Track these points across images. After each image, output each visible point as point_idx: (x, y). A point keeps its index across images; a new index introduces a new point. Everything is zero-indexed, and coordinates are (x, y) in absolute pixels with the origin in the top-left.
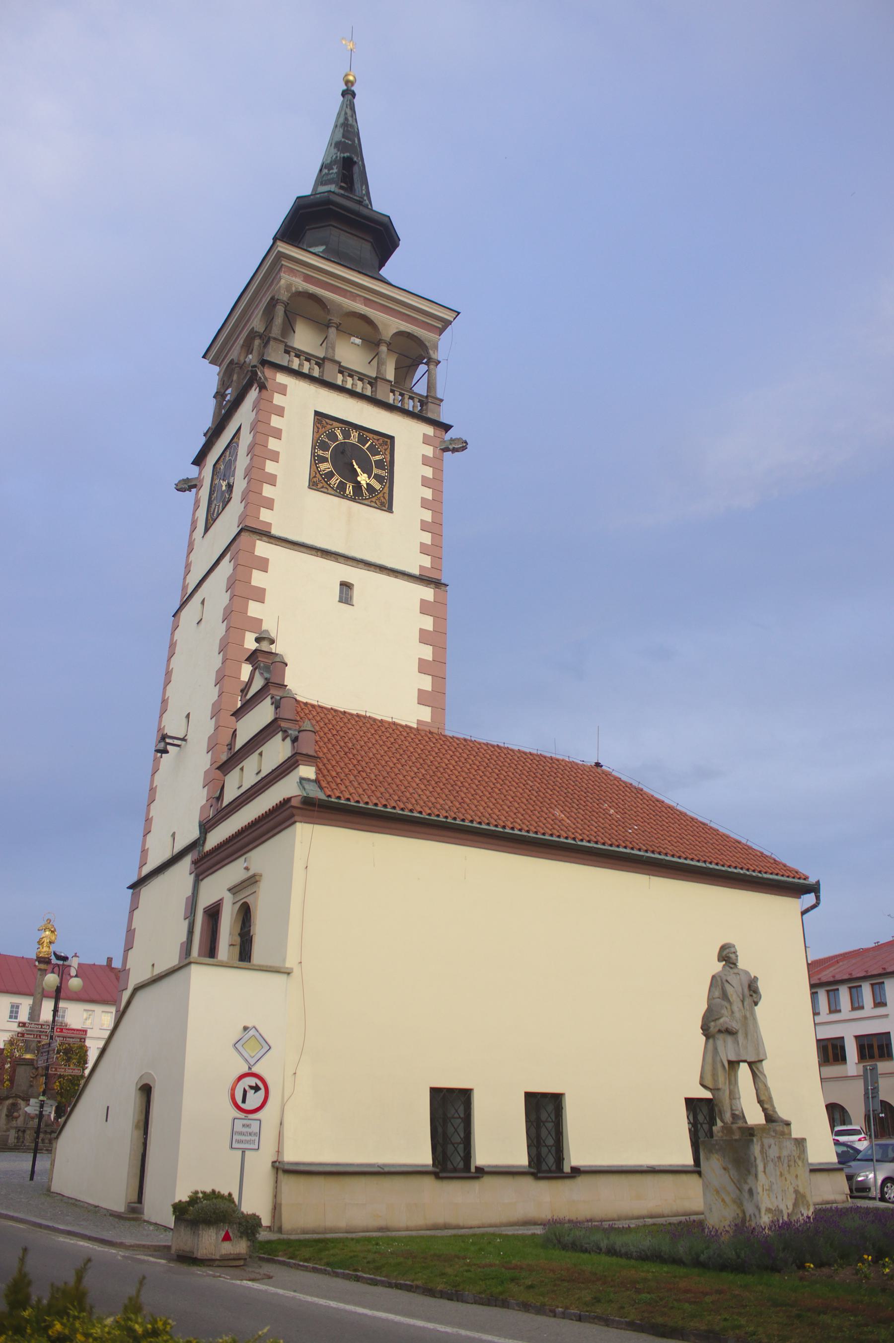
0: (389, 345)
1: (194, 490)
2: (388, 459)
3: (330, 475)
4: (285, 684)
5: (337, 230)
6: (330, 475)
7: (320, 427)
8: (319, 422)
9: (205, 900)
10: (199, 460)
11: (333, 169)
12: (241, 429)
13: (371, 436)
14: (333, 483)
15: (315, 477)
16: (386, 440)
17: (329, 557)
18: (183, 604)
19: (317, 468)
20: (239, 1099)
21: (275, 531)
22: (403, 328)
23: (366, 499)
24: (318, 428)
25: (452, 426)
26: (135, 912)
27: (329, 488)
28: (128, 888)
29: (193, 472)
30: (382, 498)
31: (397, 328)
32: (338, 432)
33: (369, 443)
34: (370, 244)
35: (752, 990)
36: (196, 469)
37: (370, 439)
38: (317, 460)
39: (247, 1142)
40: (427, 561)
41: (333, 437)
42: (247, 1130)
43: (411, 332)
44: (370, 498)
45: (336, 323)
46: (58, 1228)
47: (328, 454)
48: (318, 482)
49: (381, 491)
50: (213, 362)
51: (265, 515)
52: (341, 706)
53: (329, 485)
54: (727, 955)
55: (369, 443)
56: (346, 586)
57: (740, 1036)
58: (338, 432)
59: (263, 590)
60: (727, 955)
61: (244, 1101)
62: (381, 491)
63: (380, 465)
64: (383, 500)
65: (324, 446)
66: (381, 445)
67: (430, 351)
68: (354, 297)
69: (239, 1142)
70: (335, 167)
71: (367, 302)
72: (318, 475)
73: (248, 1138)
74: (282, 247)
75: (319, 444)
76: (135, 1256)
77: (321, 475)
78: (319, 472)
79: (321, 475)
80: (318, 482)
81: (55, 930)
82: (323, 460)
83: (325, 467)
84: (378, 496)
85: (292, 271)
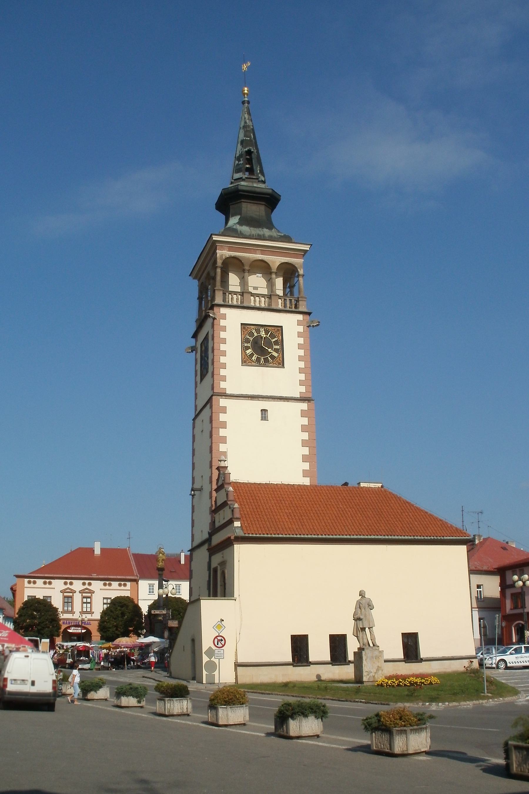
0: (276, 273)
1: (194, 352)
2: (255, 327)
3: (252, 355)
4: (93, 611)
5: (246, 203)
6: (252, 355)
7: (245, 331)
8: (244, 328)
9: (213, 565)
10: (195, 336)
11: (241, 161)
12: (192, 429)
13: (270, 328)
14: (254, 359)
15: (245, 358)
16: (278, 328)
17: (255, 399)
18: (197, 416)
19: (245, 353)
20: (216, 644)
21: (228, 392)
22: (283, 261)
23: (271, 363)
24: (244, 332)
25: (312, 313)
26: (192, 562)
27: (252, 362)
28: (188, 551)
29: (192, 342)
30: (279, 361)
31: (280, 262)
32: (254, 331)
33: (270, 332)
34: (264, 206)
35: (370, 606)
36: (193, 340)
37: (270, 330)
38: (244, 349)
39: (220, 656)
40: (303, 389)
41: (251, 334)
42: (219, 653)
43: (287, 262)
44: (273, 362)
45: (247, 270)
46: (339, 739)
47: (251, 339)
48: (246, 361)
49: (278, 357)
50: (194, 278)
51: (223, 385)
52: (258, 482)
53: (252, 361)
54: (362, 594)
55: (270, 332)
56: (264, 412)
57: (364, 620)
58: (254, 331)
59: (225, 422)
60: (362, 594)
61: (218, 644)
62: (278, 357)
63: (276, 343)
64: (280, 362)
65: (247, 341)
66: (276, 332)
67: (298, 270)
68: (255, 252)
69: (217, 656)
70: (241, 159)
71: (263, 253)
72: (246, 357)
73: (220, 655)
74: (215, 237)
75: (245, 340)
76: (208, 691)
77: (248, 356)
78: (246, 355)
79: (248, 356)
80: (246, 361)
81: (164, 553)
82: (247, 348)
83: (249, 351)
84: (277, 360)
85: (222, 249)
